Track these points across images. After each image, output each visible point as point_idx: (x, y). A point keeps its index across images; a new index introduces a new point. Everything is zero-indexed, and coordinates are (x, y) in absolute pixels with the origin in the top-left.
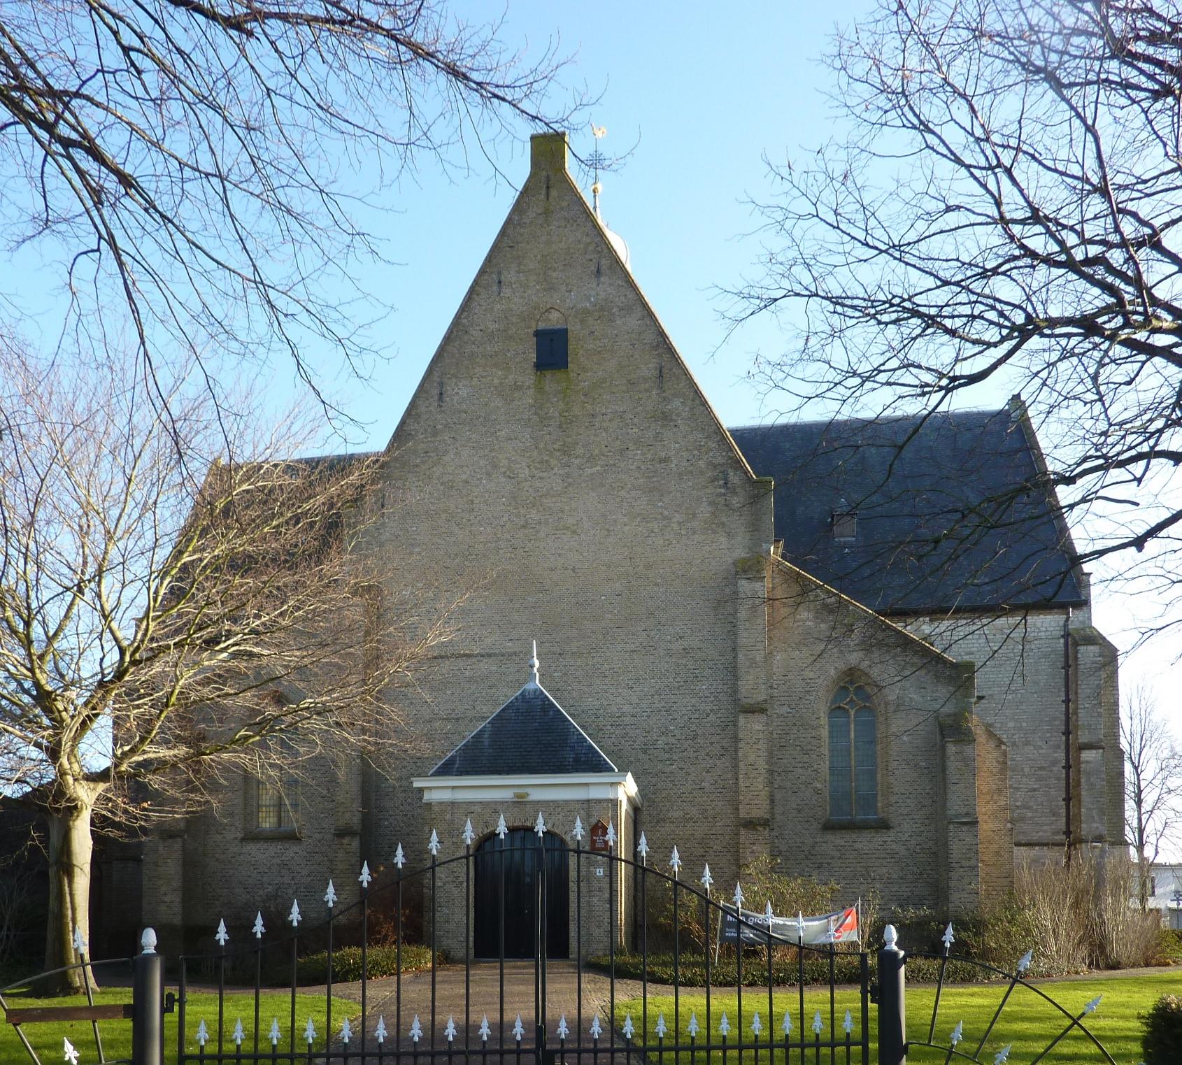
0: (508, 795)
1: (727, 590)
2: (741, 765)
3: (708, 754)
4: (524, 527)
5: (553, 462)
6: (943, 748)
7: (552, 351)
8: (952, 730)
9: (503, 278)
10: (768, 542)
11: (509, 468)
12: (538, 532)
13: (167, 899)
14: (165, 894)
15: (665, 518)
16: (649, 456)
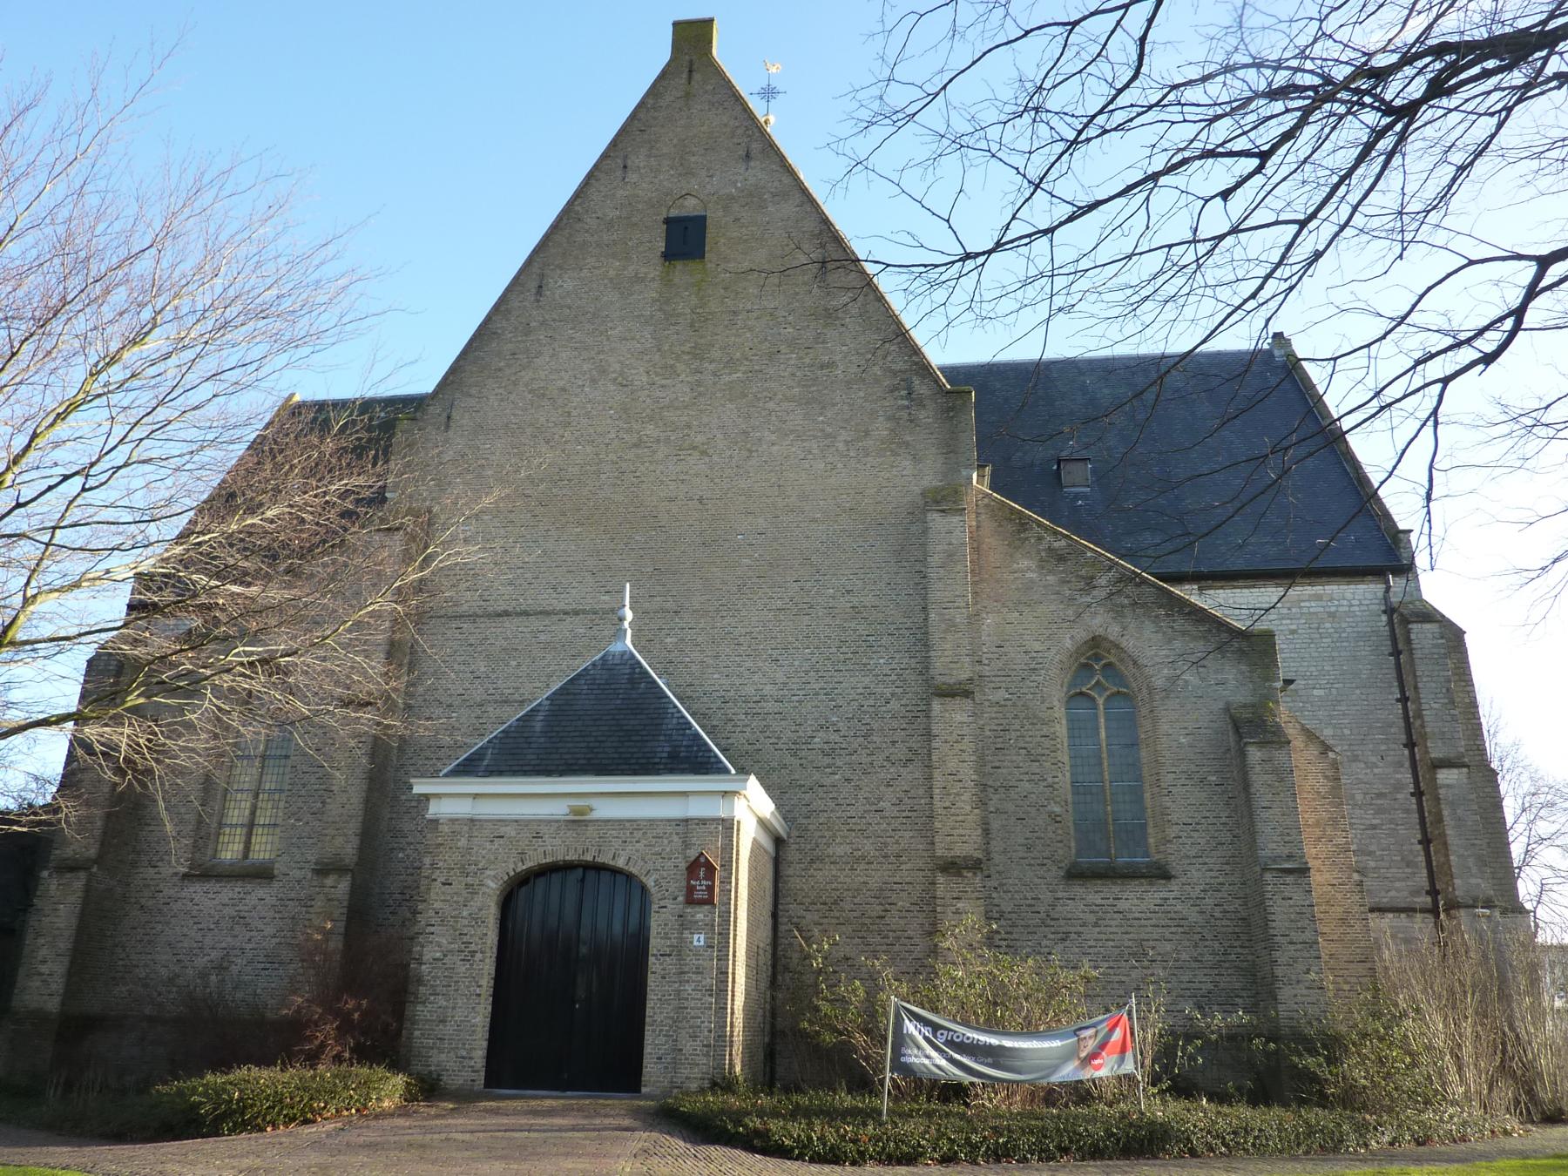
0: (559, 809)
1: (913, 528)
2: (937, 774)
3: (888, 759)
4: (636, 446)
5: (680, 367)
6: (1242, 754)
7: (685, 239)
8: (1250, 727)
9: (629, 163)
10: (970, 467)
11: (621, 374)
12: (654, 452)
13: (44, 969)
14: (44, 962)
15: (828, 436)
16: (807, 361)
